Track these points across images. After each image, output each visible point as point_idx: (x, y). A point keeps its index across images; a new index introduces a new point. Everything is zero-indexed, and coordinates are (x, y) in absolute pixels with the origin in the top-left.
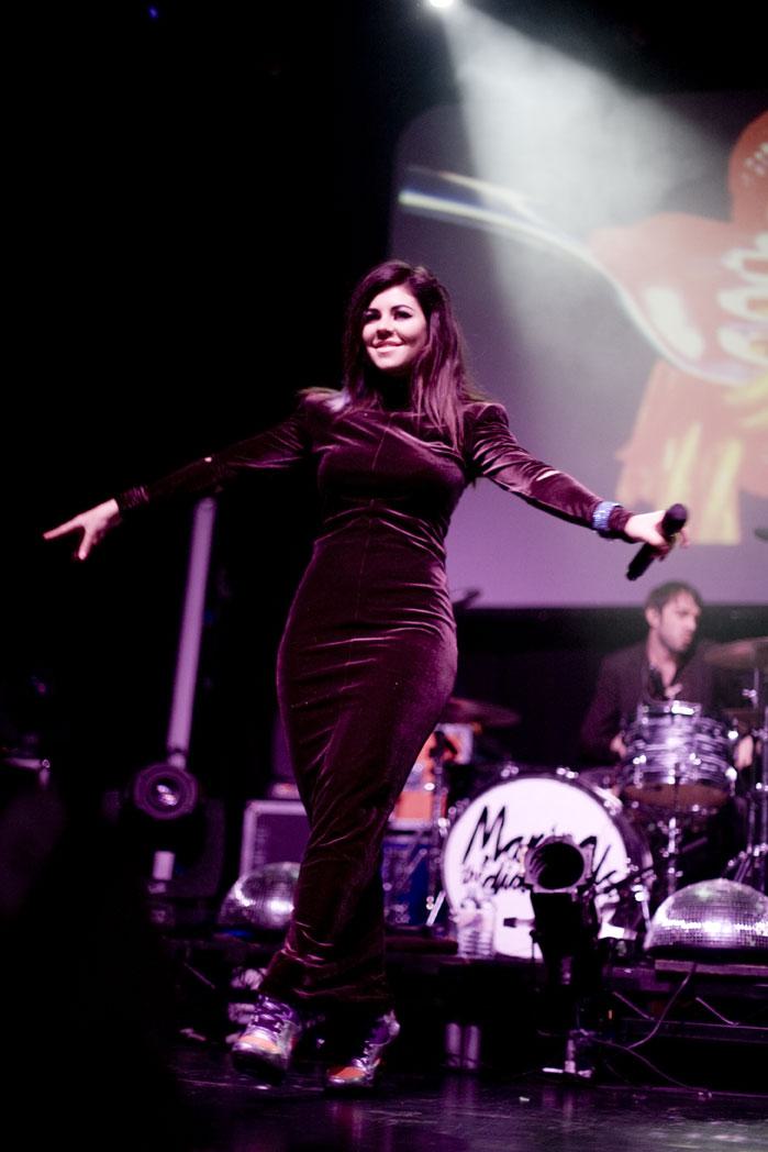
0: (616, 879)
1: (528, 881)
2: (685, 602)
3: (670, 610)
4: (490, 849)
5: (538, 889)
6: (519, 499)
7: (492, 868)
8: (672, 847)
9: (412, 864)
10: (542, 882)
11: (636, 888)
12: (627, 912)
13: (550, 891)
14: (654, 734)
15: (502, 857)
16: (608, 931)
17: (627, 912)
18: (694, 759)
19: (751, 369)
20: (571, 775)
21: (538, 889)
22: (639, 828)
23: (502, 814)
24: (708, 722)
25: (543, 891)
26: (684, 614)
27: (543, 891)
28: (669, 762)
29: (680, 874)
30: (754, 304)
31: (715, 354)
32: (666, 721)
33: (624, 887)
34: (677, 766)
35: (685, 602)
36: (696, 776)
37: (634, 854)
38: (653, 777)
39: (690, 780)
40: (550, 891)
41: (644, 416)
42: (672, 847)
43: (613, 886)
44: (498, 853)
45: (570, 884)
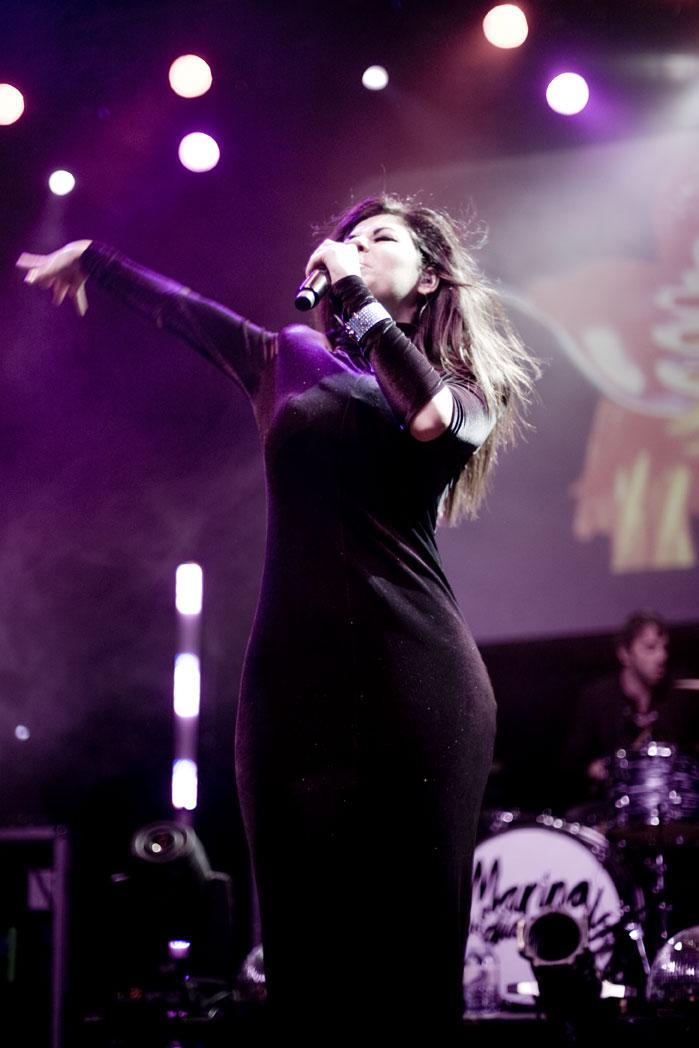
0: (612, 920)
1: (530, 953)
2: (650, 634)
3: (639, 648)
4: (488, 901)
5: (538, 962)
6: (449, 582)
7: (492, 919)
8: (661, 883)
9: (509, 336)
10: (542, 955)
11: (631, 926)
12: (627, 963)
13: (550, 963)
14: (635, 777)
15: (500, 909)
16: (612, 990)
17: (627, 963)
18: (675, 797)
19: (689, 400)
20: (559, 823)
21: (538, 962)
22: (623, 864)
23: (496, 867)
24: (684, 762)
25: (543, 963)
26: (651, 647)
27: (543, 963)
28: (652, 801)
29: (670, 909)
30: (688, 338)
31: (655, 388)
32: (644, 763)
33: (619, 930)
34: (659, 807)
35: (650, 634)
36: (678, 814)
37: (624, 894)
38: (637, 813)
39: (672, 820)
40: (550, 963)
41: (595, 453)
42: (661, 883)
43: (608, 929)
44: (497, 902)
45: (565, 956)
